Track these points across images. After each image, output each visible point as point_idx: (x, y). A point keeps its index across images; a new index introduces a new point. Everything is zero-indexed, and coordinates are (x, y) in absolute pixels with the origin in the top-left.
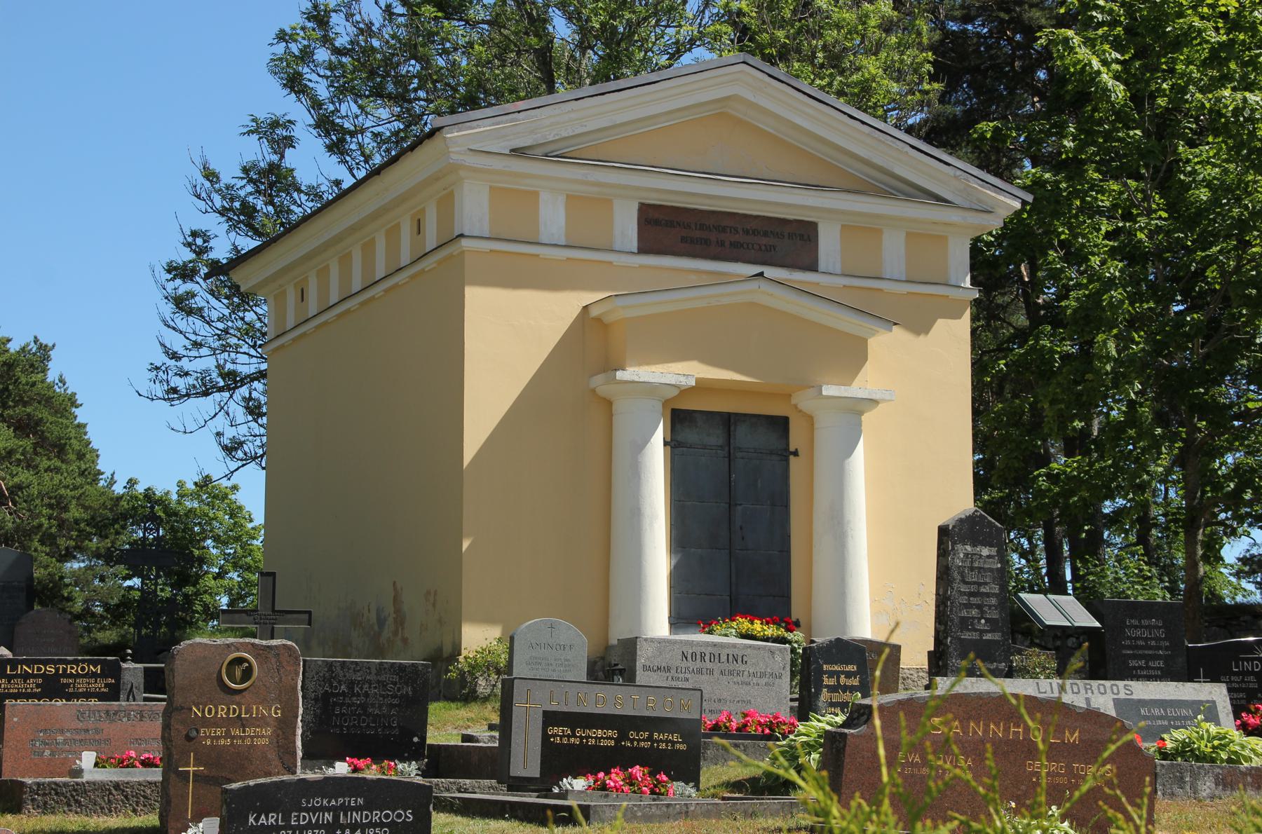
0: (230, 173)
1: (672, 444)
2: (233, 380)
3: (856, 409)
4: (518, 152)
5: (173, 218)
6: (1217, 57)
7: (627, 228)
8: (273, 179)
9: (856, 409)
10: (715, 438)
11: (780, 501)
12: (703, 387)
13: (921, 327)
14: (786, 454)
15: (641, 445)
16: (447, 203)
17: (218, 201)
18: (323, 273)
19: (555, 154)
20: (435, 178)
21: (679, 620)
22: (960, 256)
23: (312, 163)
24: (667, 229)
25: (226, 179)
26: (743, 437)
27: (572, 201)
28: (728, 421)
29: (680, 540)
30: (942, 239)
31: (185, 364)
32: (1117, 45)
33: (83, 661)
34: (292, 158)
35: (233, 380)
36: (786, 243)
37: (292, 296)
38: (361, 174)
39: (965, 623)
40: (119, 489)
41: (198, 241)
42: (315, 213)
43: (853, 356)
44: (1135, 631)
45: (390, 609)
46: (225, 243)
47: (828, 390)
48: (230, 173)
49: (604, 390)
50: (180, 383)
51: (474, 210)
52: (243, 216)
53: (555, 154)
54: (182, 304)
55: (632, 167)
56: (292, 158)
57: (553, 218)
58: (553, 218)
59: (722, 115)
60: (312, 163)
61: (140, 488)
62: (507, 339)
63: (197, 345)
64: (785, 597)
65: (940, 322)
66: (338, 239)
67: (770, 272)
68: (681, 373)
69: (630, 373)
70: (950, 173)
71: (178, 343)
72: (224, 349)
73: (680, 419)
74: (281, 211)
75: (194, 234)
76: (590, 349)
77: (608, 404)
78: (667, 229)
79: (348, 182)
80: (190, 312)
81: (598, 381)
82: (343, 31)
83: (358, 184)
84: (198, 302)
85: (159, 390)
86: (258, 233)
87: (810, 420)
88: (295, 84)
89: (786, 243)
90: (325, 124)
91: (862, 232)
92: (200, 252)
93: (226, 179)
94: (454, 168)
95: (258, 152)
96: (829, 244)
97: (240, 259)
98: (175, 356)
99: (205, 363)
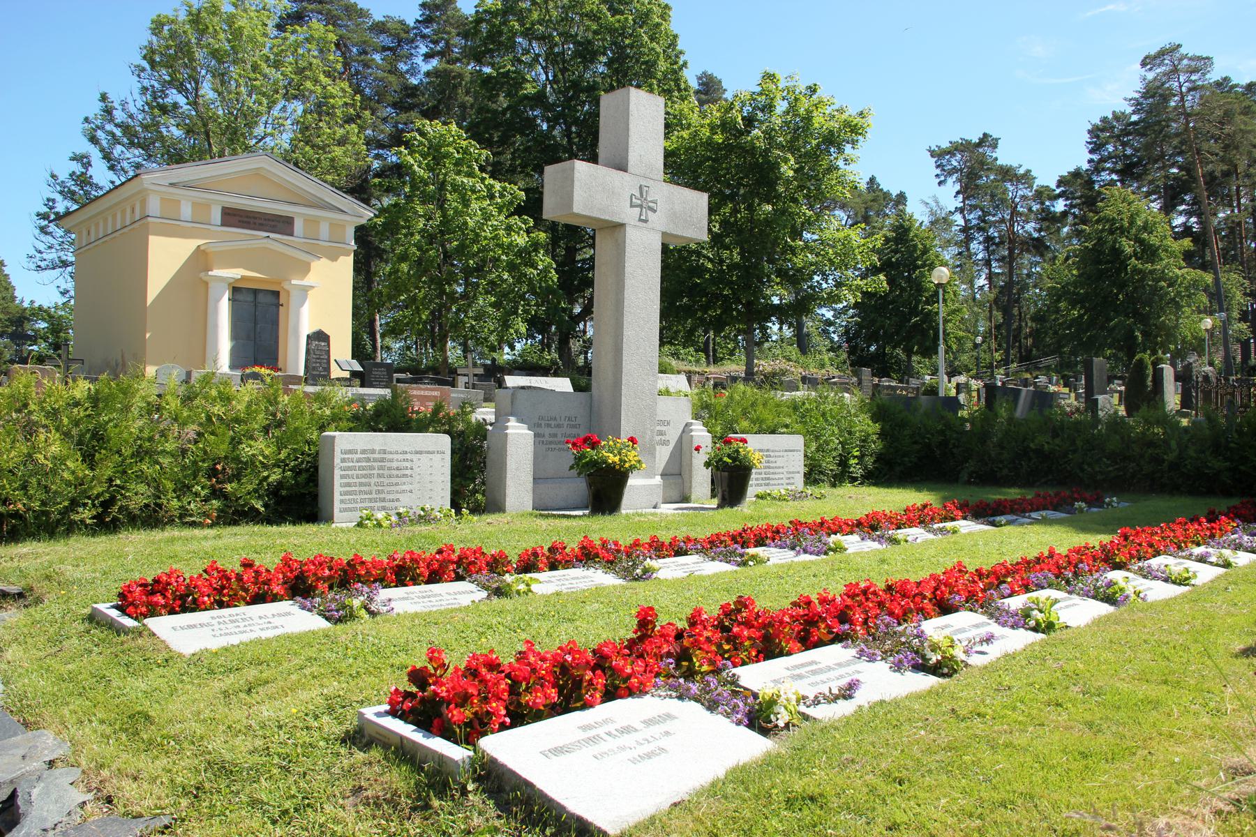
0: (63, 176)
1: (232, 300)
2: (65, 264)
3: (305, 290)
4: (172, 185)
5: (37, 195)
6: (458, 163)
7: (217, 216)
8: (83, 180)
9: (305, 290)
10: (250, 298)
11: (275, 323)
12: (244, 278)
13: (334, 258)
14: (278, 305)
15: (218, 300)
16: (144, 203)
17: (59, 188)
18: (97, 225)
19: (187, 186)
20: (139, 192)
21: (232, 367)
22: (350, 232)
23: (101, 175)
24: (235, 217)
25: (61, 178)
26: (261, 298)
27: (194, 205)
28: (255, 292)
29: (235, 336)
30: (344, 226)
31: (45, 256)
32: (424, 156)
33: (1023, 574)
34: (91, 171)
35: (65, 264)
36: (282, 225)
37: (85, 233)
38: (123, 180)
39: (314, 368)
40: (26, 305)
41: (50, 202)
42: (111, 190)
43: (305, 269)
44: (376, 372)
45: (120, 361)
46: (62, 206)
47: (294, 282)
48: (63, 176)
49: (205, 278)
50: (43, 264)
51: (154, 206)
52: (69, 195)
53: (187, 186)
54: (43, 230)
55: (219, 192)
56: (91, 171)
57: (186, 211)
58: (186, 211)
59: (257, 174)
60: (101, 175)
61: (36, 305)
62: (165, 258)
63: (50, 247)
64: (277, 359)
65: (342, 258)
66: (102, 212)
67: (272, 235)
68: (236, 273)
69: (216, 272)
70: (348, 202)
71: (42, 247)
72: (62, 250)
73: (236, 290)
74: (87, 193)
75: (48, 200)
76: (200, 261)
77: (207, 283)
78: (235, 217)
79: (118, 183)
80: (46, 233)
81: (202, 275)
82: (119, 116)
83: (123, 184)
84: (50, 229)
85: (33, 266)
86: (76, 201)
87: (288, 292)
88: (94, 140)
89: (282, 225)
90: (107, 156)
91: (311, 222)
92: (51, 208)
93: (61, 178)
94: (146, 189)
95: (77, 168)
96: (298, 226)
97: (68, 213)
98: (40, 252)
99: (52, 255)
